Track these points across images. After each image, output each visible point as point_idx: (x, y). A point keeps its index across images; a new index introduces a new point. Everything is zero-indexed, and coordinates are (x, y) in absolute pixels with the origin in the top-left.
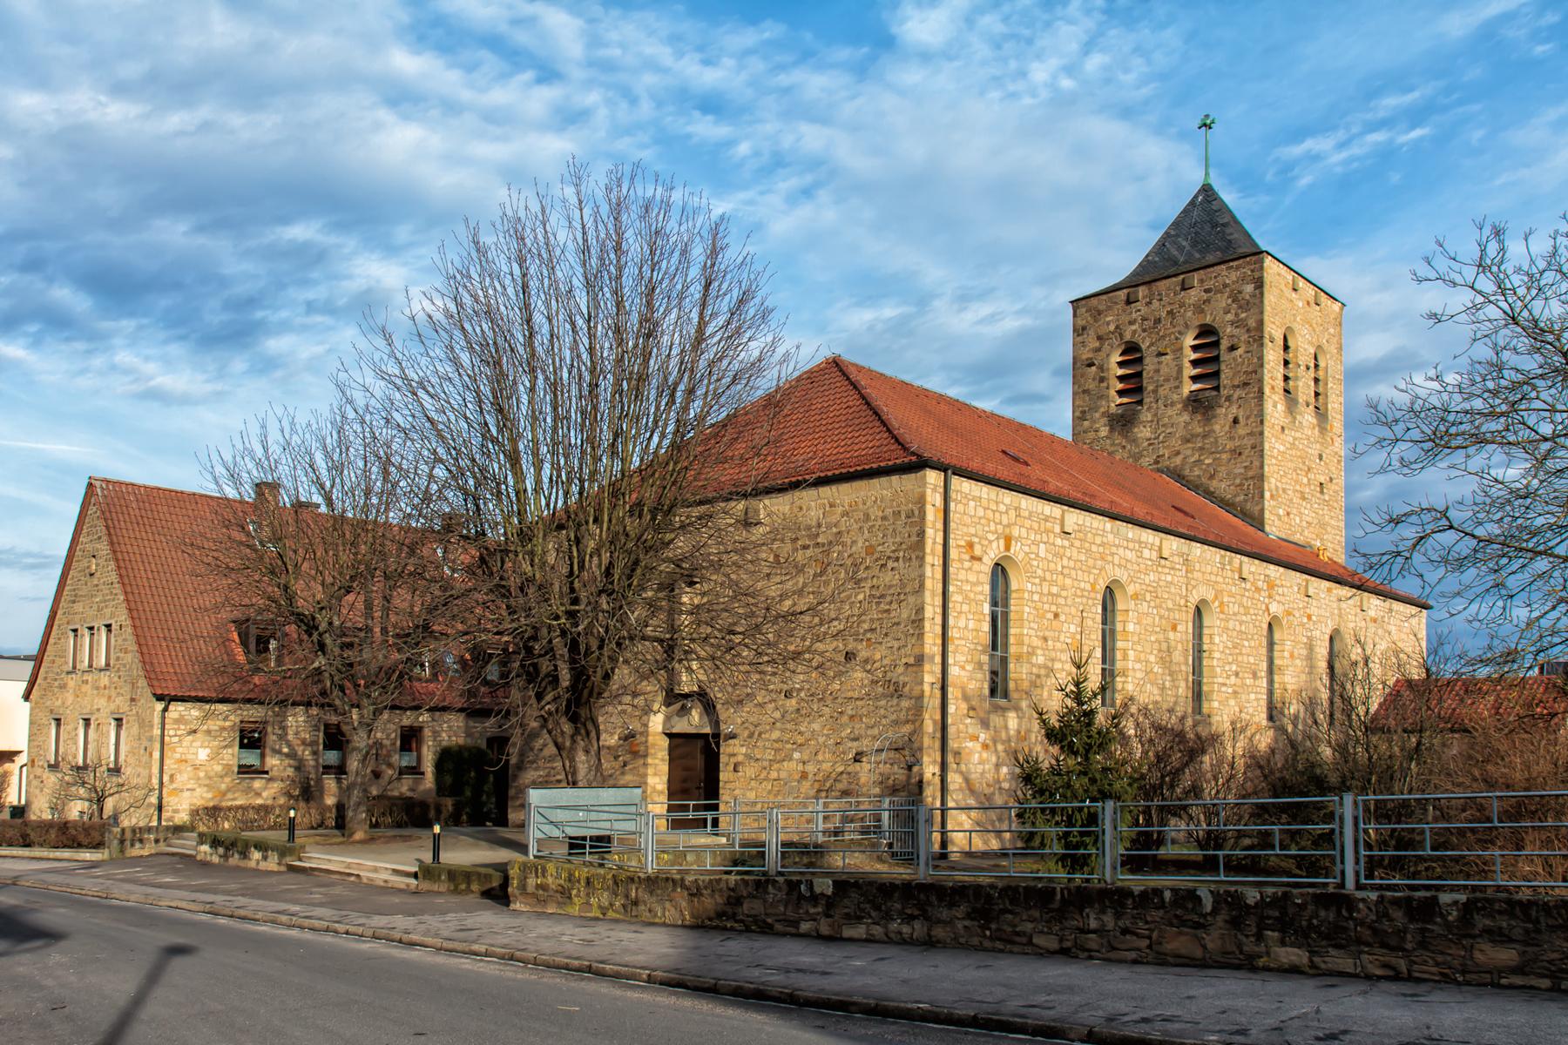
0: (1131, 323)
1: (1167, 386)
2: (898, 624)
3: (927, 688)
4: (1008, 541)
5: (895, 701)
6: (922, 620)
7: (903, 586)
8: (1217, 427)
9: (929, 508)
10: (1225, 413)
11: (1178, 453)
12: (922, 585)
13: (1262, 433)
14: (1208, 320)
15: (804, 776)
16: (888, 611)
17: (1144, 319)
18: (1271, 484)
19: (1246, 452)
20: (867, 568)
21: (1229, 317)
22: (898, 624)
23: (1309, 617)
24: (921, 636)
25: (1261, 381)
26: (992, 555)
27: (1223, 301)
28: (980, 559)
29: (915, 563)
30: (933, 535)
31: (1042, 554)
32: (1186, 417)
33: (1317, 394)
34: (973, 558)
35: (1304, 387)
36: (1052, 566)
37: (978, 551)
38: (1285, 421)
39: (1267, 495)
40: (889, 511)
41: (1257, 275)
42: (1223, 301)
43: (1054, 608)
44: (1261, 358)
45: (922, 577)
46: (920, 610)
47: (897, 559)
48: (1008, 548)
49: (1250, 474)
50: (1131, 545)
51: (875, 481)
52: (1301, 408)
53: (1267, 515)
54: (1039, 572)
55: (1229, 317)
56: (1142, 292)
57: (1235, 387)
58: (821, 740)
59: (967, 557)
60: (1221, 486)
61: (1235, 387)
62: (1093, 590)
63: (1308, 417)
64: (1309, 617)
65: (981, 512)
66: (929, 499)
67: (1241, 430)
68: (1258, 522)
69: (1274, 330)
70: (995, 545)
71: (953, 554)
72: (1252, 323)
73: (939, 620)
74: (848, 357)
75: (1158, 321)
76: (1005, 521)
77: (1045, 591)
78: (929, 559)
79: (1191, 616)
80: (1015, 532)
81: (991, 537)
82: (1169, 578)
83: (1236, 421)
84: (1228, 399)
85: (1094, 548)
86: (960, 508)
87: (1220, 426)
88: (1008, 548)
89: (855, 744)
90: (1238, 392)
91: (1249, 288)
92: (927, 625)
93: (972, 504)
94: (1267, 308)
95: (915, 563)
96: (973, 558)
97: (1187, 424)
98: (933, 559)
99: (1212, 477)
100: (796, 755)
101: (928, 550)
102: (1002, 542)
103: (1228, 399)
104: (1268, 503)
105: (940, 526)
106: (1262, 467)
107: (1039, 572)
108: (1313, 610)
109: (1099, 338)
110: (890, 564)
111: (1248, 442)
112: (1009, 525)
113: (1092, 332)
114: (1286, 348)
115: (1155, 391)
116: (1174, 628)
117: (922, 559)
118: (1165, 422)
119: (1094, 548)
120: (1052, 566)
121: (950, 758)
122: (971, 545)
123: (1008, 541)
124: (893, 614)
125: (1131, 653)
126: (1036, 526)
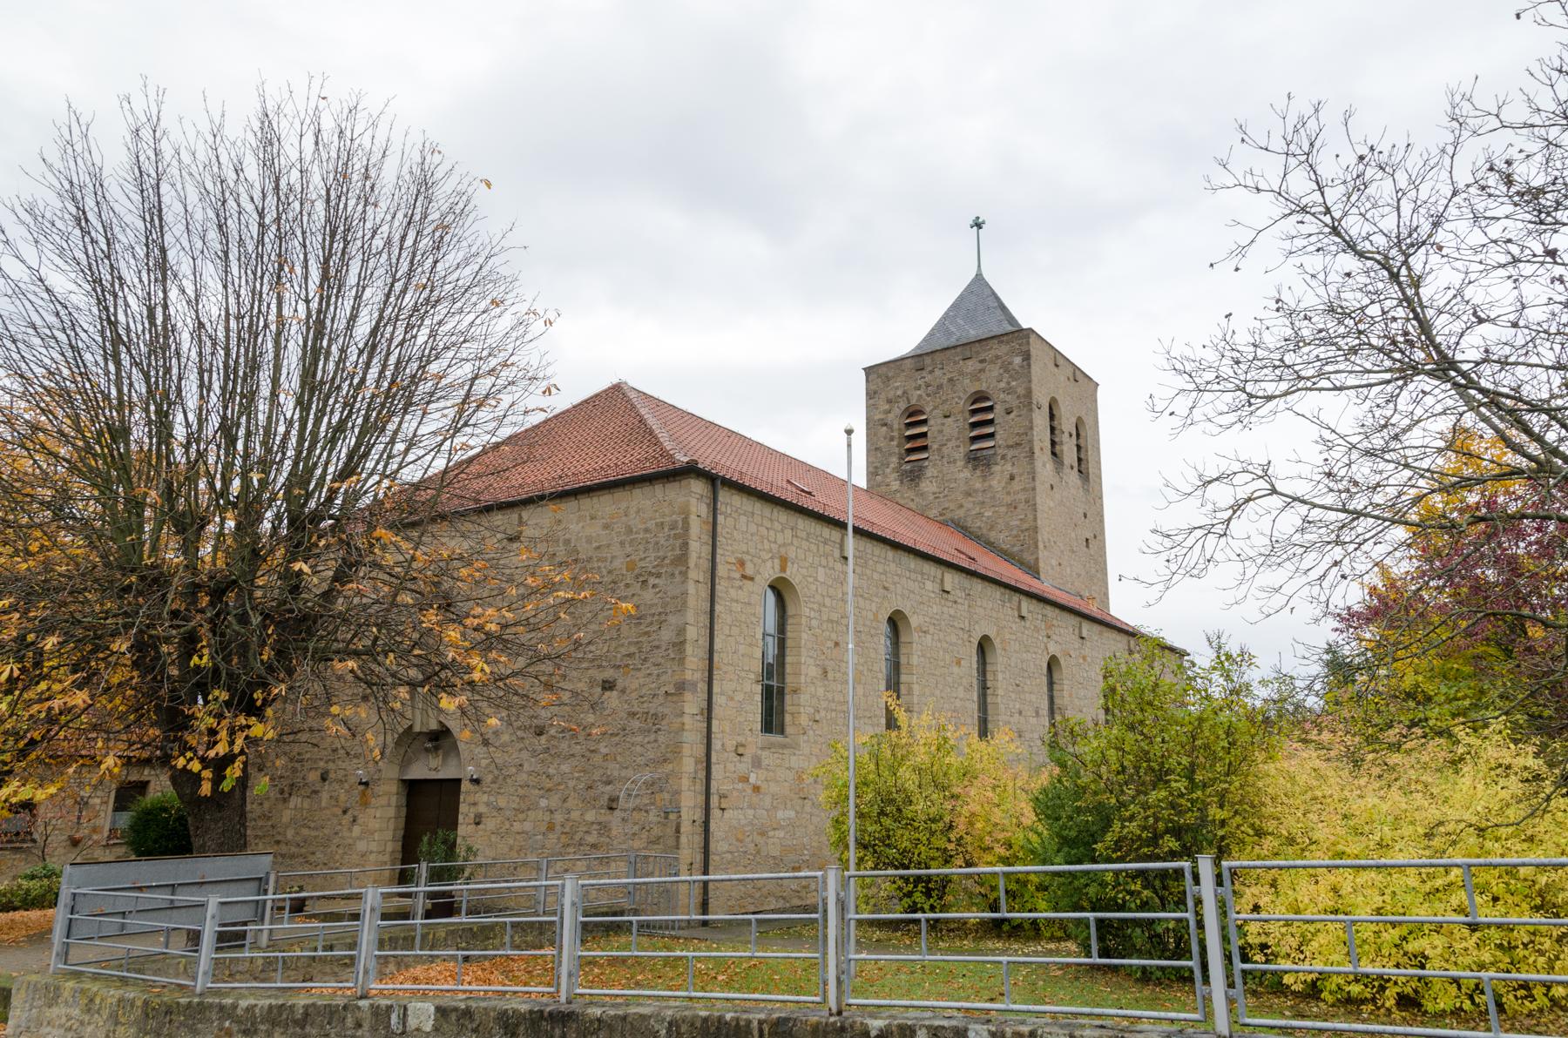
0: (919, 388)
1: (950, 445)
2: (658, 647)
3: (687, 720)
4: (784, 562)
5: (653, 737)
6: (683, 643)
7: (665, 605)
8: (994, 483)
9: (693, 517)
10: (1001, 470)
11: (961, 506)
12: (685, 603)
13: (1034, 489)
14: (984, 387)
15: (551, 827)
16: (647, 633)
17: (928, 385)
18: (1043, 536)
19: (1021, 506)
20: (627, 586)
21: (1002, 385)
22: (658, 647)
23: (1084, 658)
24: (682, 661)
25: (1031, 441)
26: (770, 572)
27: (994, 371)
28: (752, 579)
29: (678, 578)
30: (698, 549)
31: (821, 578)
32: (966, 473)
33: (1080, 460)
34: (744, 577)
35: (1069, 455)
36: (831, 591)
37: (749, 571)
38: (1055, 480)
39: (1041, 545)
40: (651, 524)
41: (1024, 348)
42: (994, 371)
43: (834, 636)
44: (1031, 421)
45: (685, 593)
46: (681, 631)
47: (659, 576)
48: (783, 569)
49: (1025, 526)
50: (913, 576)
51: (637, 492)
52: (1067, 470)
53: (1041, 565)
54: (818, 598)
55: (1002, 385)
56: (928, 360)
57: (1009, 447)
58: (571, 784)
59: (737, 575)
60: (1001, 538)
61: (1009, 447)
62: (876, 618)
63: (1073, 477)
64: (1084, 658)
65: (753, 528)
66: (693, 509)
67: (1016, 485)
68: (1034, 571)
69: (1041, 397)
70: (769, 564)
71: (722, 570)
72: (1021, 391)
73: (704, 642)
74: (641, 380)
75: (940, 387)
76: (780, 540)
77: (825, 618)
78: (693, 574)
79: (974, 651)
80: (792, 555)
81: (766, 556)
82: (952, 612)
83: (1012, 478)
84: (1003, 457)
85: (876, 576)
86: (730, 521)
87: (997, 481)
88: (783, 569)
89: (609, 788)
90: (1010, 453)
91: (1018, 360)
92: (689, 649)
93: (743, 519)
94: (1034, 379)
95: (678, 578)
96: (744, 577)
97: (967, 481)
98: (697, 573)
99: (991, 528)
100: (543, 803)
101: (692, 564)
102: (777, 561)
103: (1003, 457)
104: (1042, 554)
105: (707, 538)
106: (1035, 519)
107: (818, 598)
108: (1087, 651)
109: (889, 401)
110: (652, 581)
111: (1022, 496)
112: (784, 545)
113: (883, 396)
114: (1052, 417)
115: (939, 450)
116: (958, 663)
117: (684, 574)
118: (947, 469)
119: (876, 576)
120: (831, 591)
121: (714, 800)
122: (742, 563)
123: (784, 562)
124: (654, 636)
125: (915, 687)
126: (813, 548)
